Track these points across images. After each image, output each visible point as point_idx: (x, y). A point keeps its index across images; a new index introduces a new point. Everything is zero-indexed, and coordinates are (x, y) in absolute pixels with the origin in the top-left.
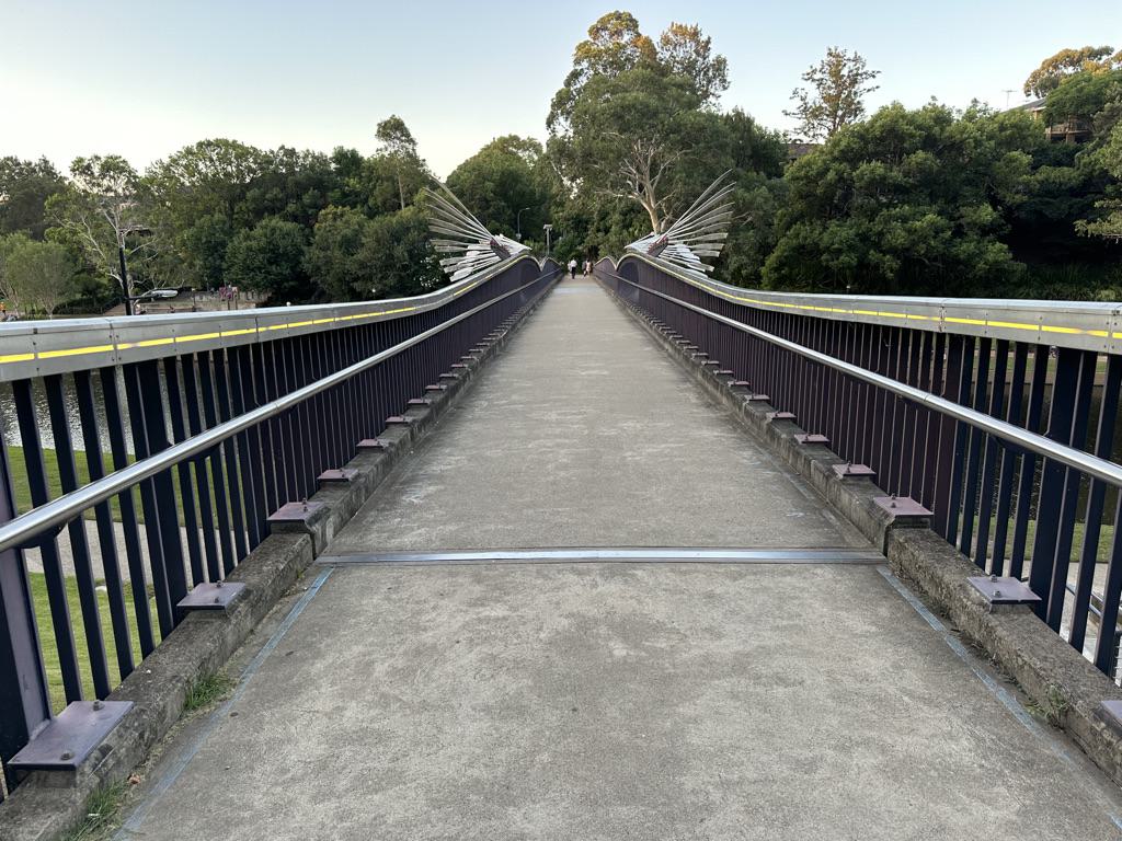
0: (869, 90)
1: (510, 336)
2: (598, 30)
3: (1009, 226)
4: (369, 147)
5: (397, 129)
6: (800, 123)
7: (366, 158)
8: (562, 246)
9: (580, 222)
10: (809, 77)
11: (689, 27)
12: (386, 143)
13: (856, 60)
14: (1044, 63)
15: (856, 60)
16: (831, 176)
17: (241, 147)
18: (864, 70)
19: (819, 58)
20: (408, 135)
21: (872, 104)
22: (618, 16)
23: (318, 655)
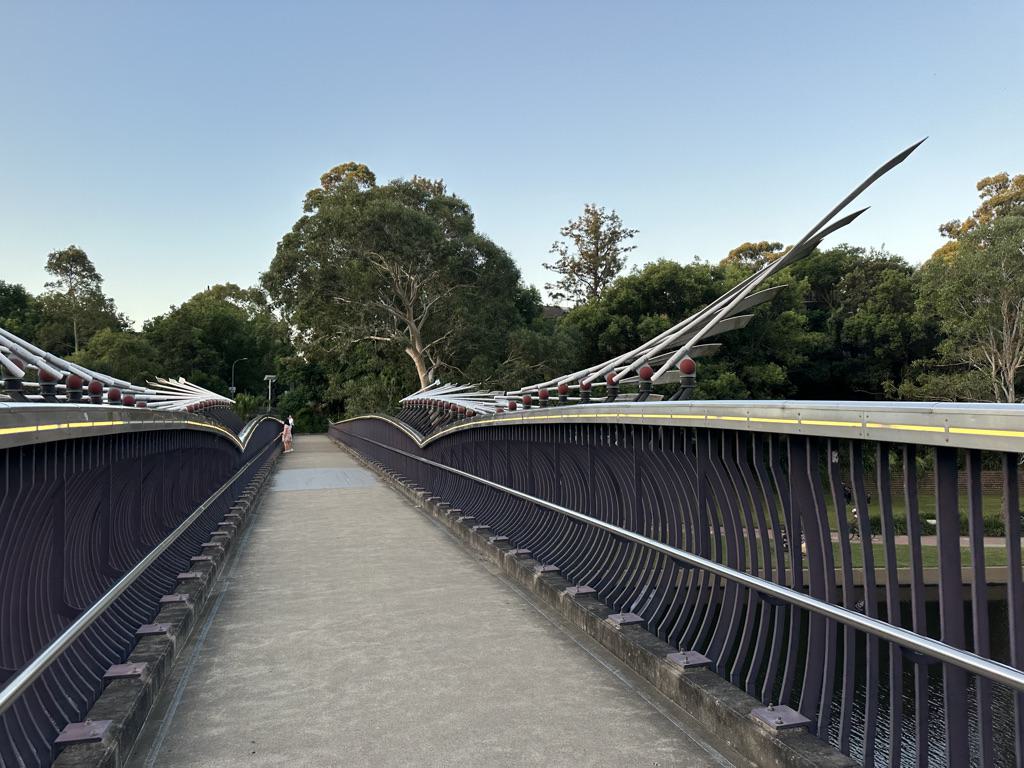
0: (626, 250)
2: (331, 179)
3: (795, 387)
5: (77, 263)
6: (562, 277)
7: (35, 296)
9: (312, 373)
10: (567, 232)
11: (432, 182)
12: (60, 278)
13: (613, 218)
14: (731, 253)
15: (613, 218)
16: (613, 328)
18: (621, 229)
19: (577, 214)
20: (91, 269)
21: (634, 260)
22: (354, 167)
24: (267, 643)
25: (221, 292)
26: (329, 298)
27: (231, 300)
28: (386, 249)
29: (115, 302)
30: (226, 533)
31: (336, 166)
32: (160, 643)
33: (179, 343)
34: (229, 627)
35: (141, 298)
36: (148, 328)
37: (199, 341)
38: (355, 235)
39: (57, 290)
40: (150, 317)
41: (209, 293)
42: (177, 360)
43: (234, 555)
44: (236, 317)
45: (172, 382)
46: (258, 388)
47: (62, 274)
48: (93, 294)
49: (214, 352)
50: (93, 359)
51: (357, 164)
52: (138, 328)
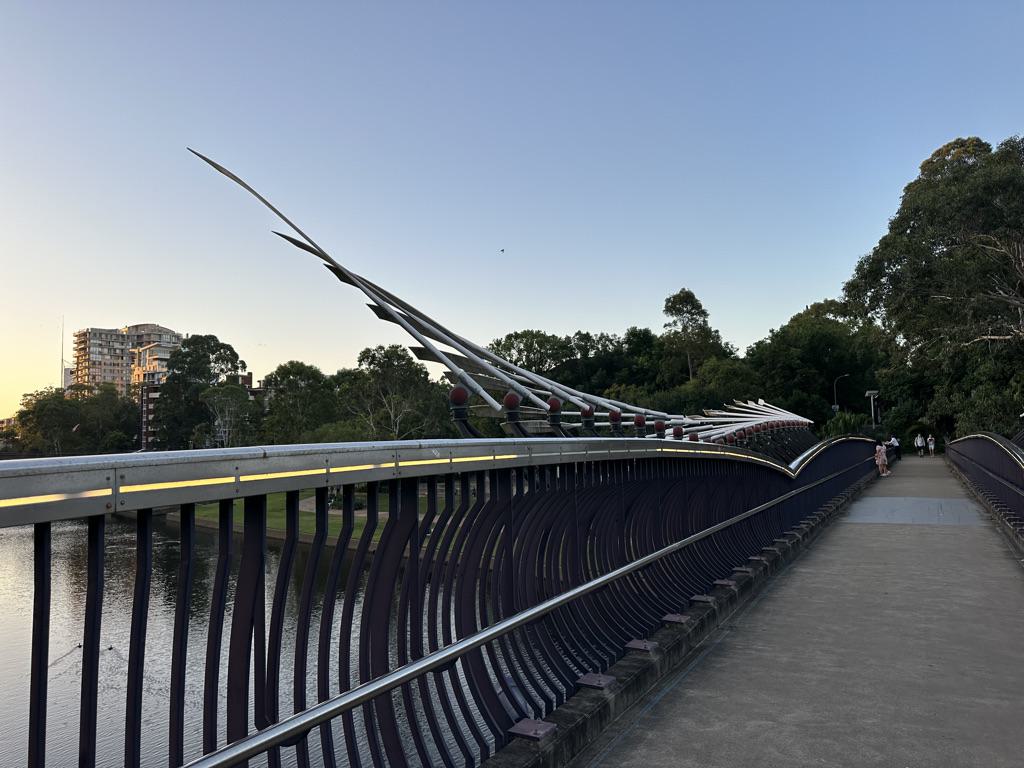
1: (846, 505)
4: (660, 325)
7: (659, 336)
8: (894, 418)
12: (675, 318)
17: (544, 336)
22: (960, 143)
23: (692, 689)
24: (717, 727)
25: (818, 309)
26: (925, 299)
27: (831, 316)
28: (996, 227)
29: (720, 333)
30: (749, 570)
31: (937, 149)
32: (593, 700)
33: (779, 365)
34: (691, 693)
35: (743, 326)
36: (751, 352)
37: (798, 361)
38: (951, 218)
39: (673, 329)
40: (752, 342)
41: (808, 312)
42: (778, 381)
43: (755, 597)
44: (834, 333)
45: (751, 404)
46: (862, 407)
47: (676, 314)
48: (700, 327)
49: (813, 371)
50: (703, 386)
51: (966, 138)
52: (742, 354)
